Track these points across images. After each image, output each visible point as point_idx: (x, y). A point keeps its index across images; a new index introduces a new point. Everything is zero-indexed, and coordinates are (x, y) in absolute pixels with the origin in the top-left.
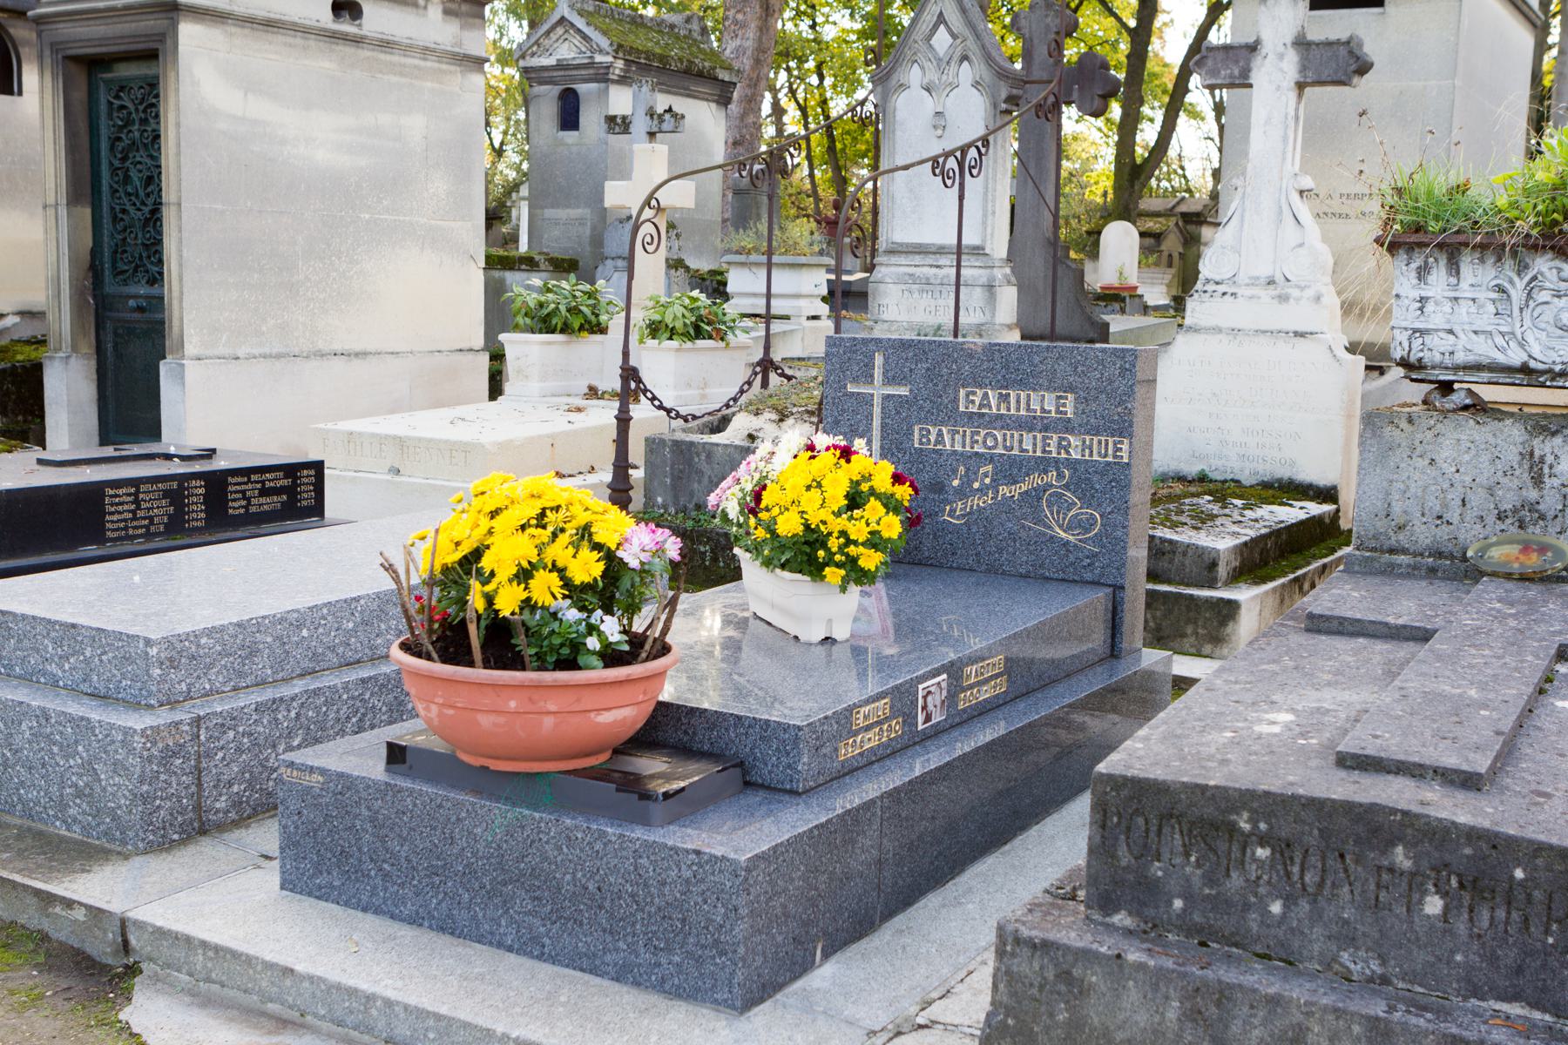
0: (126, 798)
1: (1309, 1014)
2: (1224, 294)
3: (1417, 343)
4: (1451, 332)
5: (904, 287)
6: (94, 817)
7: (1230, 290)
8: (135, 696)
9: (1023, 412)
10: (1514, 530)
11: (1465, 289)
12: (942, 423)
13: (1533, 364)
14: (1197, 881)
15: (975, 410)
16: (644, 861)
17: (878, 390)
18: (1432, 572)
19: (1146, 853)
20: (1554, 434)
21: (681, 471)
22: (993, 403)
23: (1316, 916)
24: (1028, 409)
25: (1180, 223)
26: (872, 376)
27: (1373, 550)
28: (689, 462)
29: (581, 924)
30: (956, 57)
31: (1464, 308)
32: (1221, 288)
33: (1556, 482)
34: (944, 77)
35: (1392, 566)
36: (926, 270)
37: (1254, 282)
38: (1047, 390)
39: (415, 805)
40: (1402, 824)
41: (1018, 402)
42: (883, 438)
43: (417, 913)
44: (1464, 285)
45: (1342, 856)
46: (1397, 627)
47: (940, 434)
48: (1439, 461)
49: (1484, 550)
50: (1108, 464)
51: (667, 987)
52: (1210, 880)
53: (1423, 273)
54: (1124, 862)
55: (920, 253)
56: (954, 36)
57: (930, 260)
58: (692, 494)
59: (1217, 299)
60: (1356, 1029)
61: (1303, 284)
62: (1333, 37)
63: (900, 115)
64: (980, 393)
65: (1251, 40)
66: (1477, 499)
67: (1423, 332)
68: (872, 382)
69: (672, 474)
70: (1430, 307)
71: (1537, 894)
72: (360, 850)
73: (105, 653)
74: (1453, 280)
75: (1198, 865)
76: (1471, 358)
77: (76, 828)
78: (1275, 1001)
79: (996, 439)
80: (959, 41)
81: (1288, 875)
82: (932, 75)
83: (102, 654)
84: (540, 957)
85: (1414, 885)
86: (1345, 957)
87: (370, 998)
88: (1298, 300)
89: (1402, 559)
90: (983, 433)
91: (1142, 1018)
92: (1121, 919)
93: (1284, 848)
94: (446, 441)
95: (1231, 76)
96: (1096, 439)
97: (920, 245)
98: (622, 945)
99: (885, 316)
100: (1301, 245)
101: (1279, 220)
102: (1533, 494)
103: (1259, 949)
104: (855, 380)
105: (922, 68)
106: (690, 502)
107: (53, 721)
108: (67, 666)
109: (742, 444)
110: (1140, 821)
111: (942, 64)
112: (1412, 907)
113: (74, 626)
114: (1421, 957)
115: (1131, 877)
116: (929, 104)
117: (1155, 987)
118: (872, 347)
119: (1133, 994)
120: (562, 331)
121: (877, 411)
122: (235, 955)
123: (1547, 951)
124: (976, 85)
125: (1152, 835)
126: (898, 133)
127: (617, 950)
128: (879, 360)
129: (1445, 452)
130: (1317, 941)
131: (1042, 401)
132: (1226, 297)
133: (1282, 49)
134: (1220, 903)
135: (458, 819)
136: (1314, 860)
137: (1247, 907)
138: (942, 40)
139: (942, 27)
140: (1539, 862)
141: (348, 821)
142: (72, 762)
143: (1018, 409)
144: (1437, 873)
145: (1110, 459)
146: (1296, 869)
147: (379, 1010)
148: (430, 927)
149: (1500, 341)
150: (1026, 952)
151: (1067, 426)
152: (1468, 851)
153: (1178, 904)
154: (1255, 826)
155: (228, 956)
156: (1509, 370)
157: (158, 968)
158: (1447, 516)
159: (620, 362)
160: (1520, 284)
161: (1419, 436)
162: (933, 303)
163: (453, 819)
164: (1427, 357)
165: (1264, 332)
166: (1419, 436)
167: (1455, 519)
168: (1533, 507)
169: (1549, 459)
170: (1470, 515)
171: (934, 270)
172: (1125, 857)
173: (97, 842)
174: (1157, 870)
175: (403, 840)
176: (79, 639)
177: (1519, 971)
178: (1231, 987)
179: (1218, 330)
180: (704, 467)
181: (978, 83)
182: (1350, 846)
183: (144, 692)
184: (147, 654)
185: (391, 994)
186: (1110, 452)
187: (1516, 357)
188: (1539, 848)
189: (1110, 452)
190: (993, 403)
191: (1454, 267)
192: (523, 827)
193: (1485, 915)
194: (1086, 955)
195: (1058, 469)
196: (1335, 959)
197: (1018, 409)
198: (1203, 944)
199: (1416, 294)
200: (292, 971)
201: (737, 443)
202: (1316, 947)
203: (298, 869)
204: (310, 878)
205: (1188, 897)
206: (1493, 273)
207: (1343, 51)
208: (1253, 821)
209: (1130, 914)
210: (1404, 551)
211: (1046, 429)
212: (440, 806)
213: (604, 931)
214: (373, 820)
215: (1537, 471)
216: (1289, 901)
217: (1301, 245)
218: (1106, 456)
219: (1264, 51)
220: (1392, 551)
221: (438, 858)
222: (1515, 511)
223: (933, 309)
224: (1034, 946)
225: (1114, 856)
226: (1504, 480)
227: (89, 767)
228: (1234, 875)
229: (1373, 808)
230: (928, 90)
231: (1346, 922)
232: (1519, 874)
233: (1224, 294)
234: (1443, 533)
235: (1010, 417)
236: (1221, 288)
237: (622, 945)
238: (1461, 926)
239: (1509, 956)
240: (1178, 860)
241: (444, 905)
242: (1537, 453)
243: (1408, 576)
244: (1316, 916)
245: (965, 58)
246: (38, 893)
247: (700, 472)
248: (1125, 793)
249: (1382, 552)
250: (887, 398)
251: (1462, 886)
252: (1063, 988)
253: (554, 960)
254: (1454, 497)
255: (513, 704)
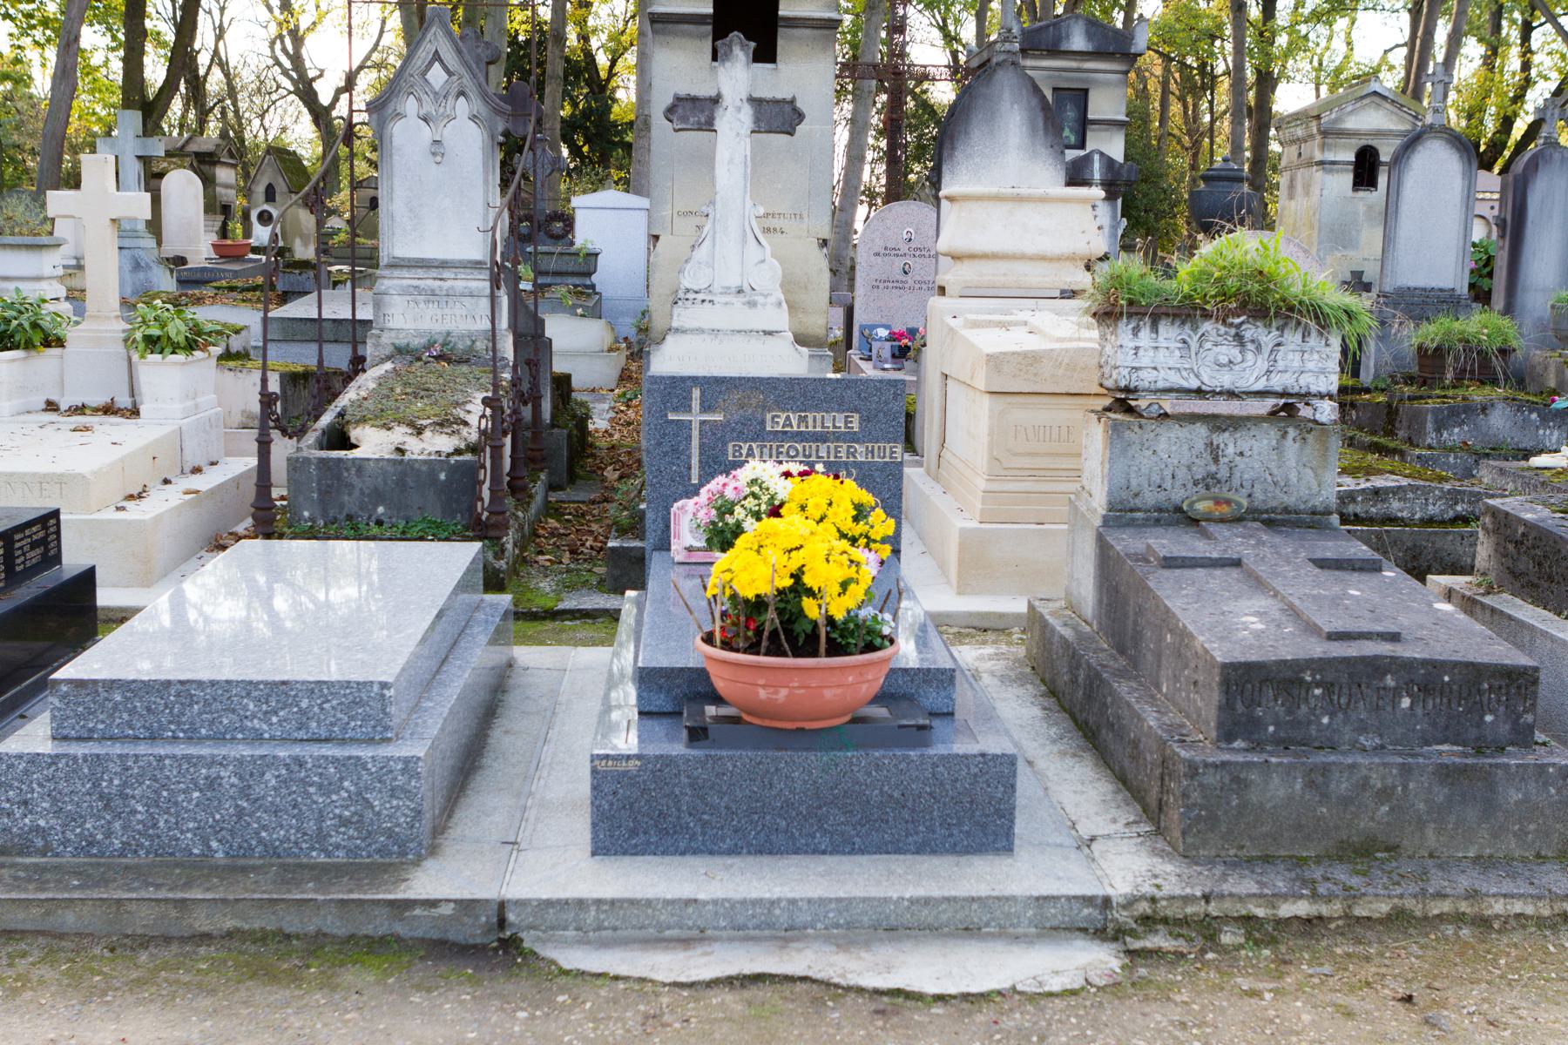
0: (406, 816)
1: (1370, 769)
2: (703, 301)
3: (1134, 377)
4: (1155, 368)
5: (409, 298)
6: (364, 840)
7: (708, 298)
8: (368, 733)
9: (819, 429)
10: (1203, 491)
11: (1162, 342)
12: (753, 440)
13: (1204, 387)
14: (1282, 714)
15: (780, 429)
16: (941, 769)
17: (695, 417)
18: (1157, 521)
19: (1253, 703)
20: (1224, 431)
21: (328, 486)
22: (794, 423)
23: (1347, 720)
24: (823, 427)
25: (195, 164)
26: (690, 406)
27: (1120, 510)
28: (339, 477)
29: (887, 821)
30: (454, 91)
31: (1162, 352)
32: (700, 297)
33: (1226, 460)
34: (442, 110)
35: (1133, 520)
36: (430, 283)
37: (726, 291)
38: (838, 411)
39: (735, 766)
40: (1390, 663)
41: (815, 421)
42: (701, 454)
43: (736, 845)
44: (1161, 339)
45: (1360, 686)
46: (1216, 559)
47: (750, 448)
48: (1159, 451)
49: (1191, 505)
50: (886, 463)
51: (958, 849)
52: (1290, 712)
53: (1136, 331)
54: (1240, 712)
55: (421, 267)
56: (449, 73)
57: (434, 273)
58: (342, 506)
59: (698, 305)
60: (1394, 771)
61: (766, 292)
62: (779, 96)
63: (397, 141)
64: (784, 416)
65: (713, 93)
66: (1182, 474)
67: (1137, 369)
68: (690, 411)
69: (319, 490)
70: (1141, 353)
71: (1455, 687)
72: (679, 810)
73: (328, 701)
74: (1154, 336)
75: (1283, 705)
76: (1167, 385)
77: (341, 853)
78: (1353, 766)
79: (797, 450)
80: (455, 78)
81: (1331, 700)
82: (429, 107)
83: (323, 703)
84: (852, 852)
85: (1396, 693)
86: (1362, 738)
87: (773, 903)
88: (764, 305)
89: (1139, 515)
90: (786, 446)
91: (1281, 793)
92: (1238, 744)
93: (1328, 687)
94: (34, 474)
95: (699, 123)
96: (876, 446)
97: (423, 260)
98: (921, 828)
99: (391, 325)
100: (763, 261)
101: (744, 241)
102: (1213, 468)
103: (1316, 744)
104: (675, 410)
105: (419, 100)
106: (340, 513)
107: (309, 766)
108: (275, 719)
109: (392, 457)
110: (1249, 686)
111: (439, 97)
112: (1395, 704)
113: (284, 683)
114: (1400, 731)
115: (1243, 719)
116: (426, 133)
117: (1288, 774)
118: (689, 383)
119: (1276, 779)
120: (26, 348)
121: (695, 433)
122: (633, 902)
123: (1460, 715)
124: (473, 118)
125: (1256, 693)
126: (396, 158)
127: (917, 833)
128: (696, 393)
129: (1162, 445)
130: (1347, 734)
131: (834, 420)
132: (706, 304)
133: (739, 103)
134: (1296, 724)
135: (777, 769)
136: (1345, 691)
137: (1309, 723)
138: (437, 75)
139: (437, 64)
140: (1456, 671)
141: (667, 790)
142: (334, 797)
143: (815, 427)
144: (1406, 687)
145: (887, 460)
146: (1336, 697)
147: (783, 910)
148: (749, 853)
149: (1185, 374)
150: (1212, 770)
151: (851, 438)
152: (1422, 671)
153: (1271, 729)
154: (1314, 678)
155: (626, 905)
156: (1188, 391)
157: (540, 934)
158: (1164, 486)
159: (258, 388)
160: (1196, 338)
161: (1146, 436)
162: (439, 312)
163: (773, 770)
164: (1141, 385)
165: (739, 332)
166: (1146, 436)
167: (1169, 488)
168: (1213, 476)
169: (1222, 446)
170: (1178, 483)
171: (438, 283)
172: (1240, 708)
173: (368, 860)
174: (1259, 712)
175: (722, 794)
176: (293, 693)
177: (1447, 727)
178: (1329, 764)
179: (700, 331)
180: (355, 480)
181: (475, 116)
182: (1364, 680)
183: (379, 728)
184: (383, 696)
185: (791, 895)
186: (888, 454)
187: (1194, 383)
188: (1456, 664)
189: (888, 454)
190: (794, 423)
191: (1155, 328)
192: (836, 765)
193: (1431, 702)
194: (1248, 765)
195: (847, 469)
196: (1357, 741)
197: (815, 427)
198: (1287, 748)
199: (1132, 344)
200: (696, 901)
201: (387, 457)
202: (1347, 737)
203: (611, 836)
204: (625, 841)
205: (1276, 724)
206: (1178, 331)
207: (787, 108)
208: (1313, 675)
209: (1244, 740)
210: (1139, 510)
211: (838, 439)
212: (760, 763)
213: (907, 822)
214: (691, 785)
215: (1215, 453)
216: (1332, 715)
217: (763, 261)
218: (810, 456)
219: (724, 104)
220: (1131, 510)
221: (757, 801)
222: (1204, 479)
223: (440, 317)
224: (1217, 766)
225: (1233, 709)
226: (1197, 461)
227: (359, 797)
228: (1303, 707)
229: (1376, 657)
230: (425, 120)
231: (1362, 720)
232: (1446, 679)
233: (703, 301)
234: (1162, 496)
235: (808, 433)
236: (700, 297)
237: (921, 828)
238: (1419, 711)
239: (1442, 721)
240: (1272, 704)
241: (762, 834)
242: (1215, 443)
243: (1144, 526)
244: (1347, 720)
245: (462, 93)
246: (392, 903)
247: (351, 486)
248: (1240, 672)
249: (1125, 511)
250: (703, 423)
251: (1419, 690)
252: (1235, 786)
253: (862, 852)
254: (1168, 473)
255: (851, 679)
